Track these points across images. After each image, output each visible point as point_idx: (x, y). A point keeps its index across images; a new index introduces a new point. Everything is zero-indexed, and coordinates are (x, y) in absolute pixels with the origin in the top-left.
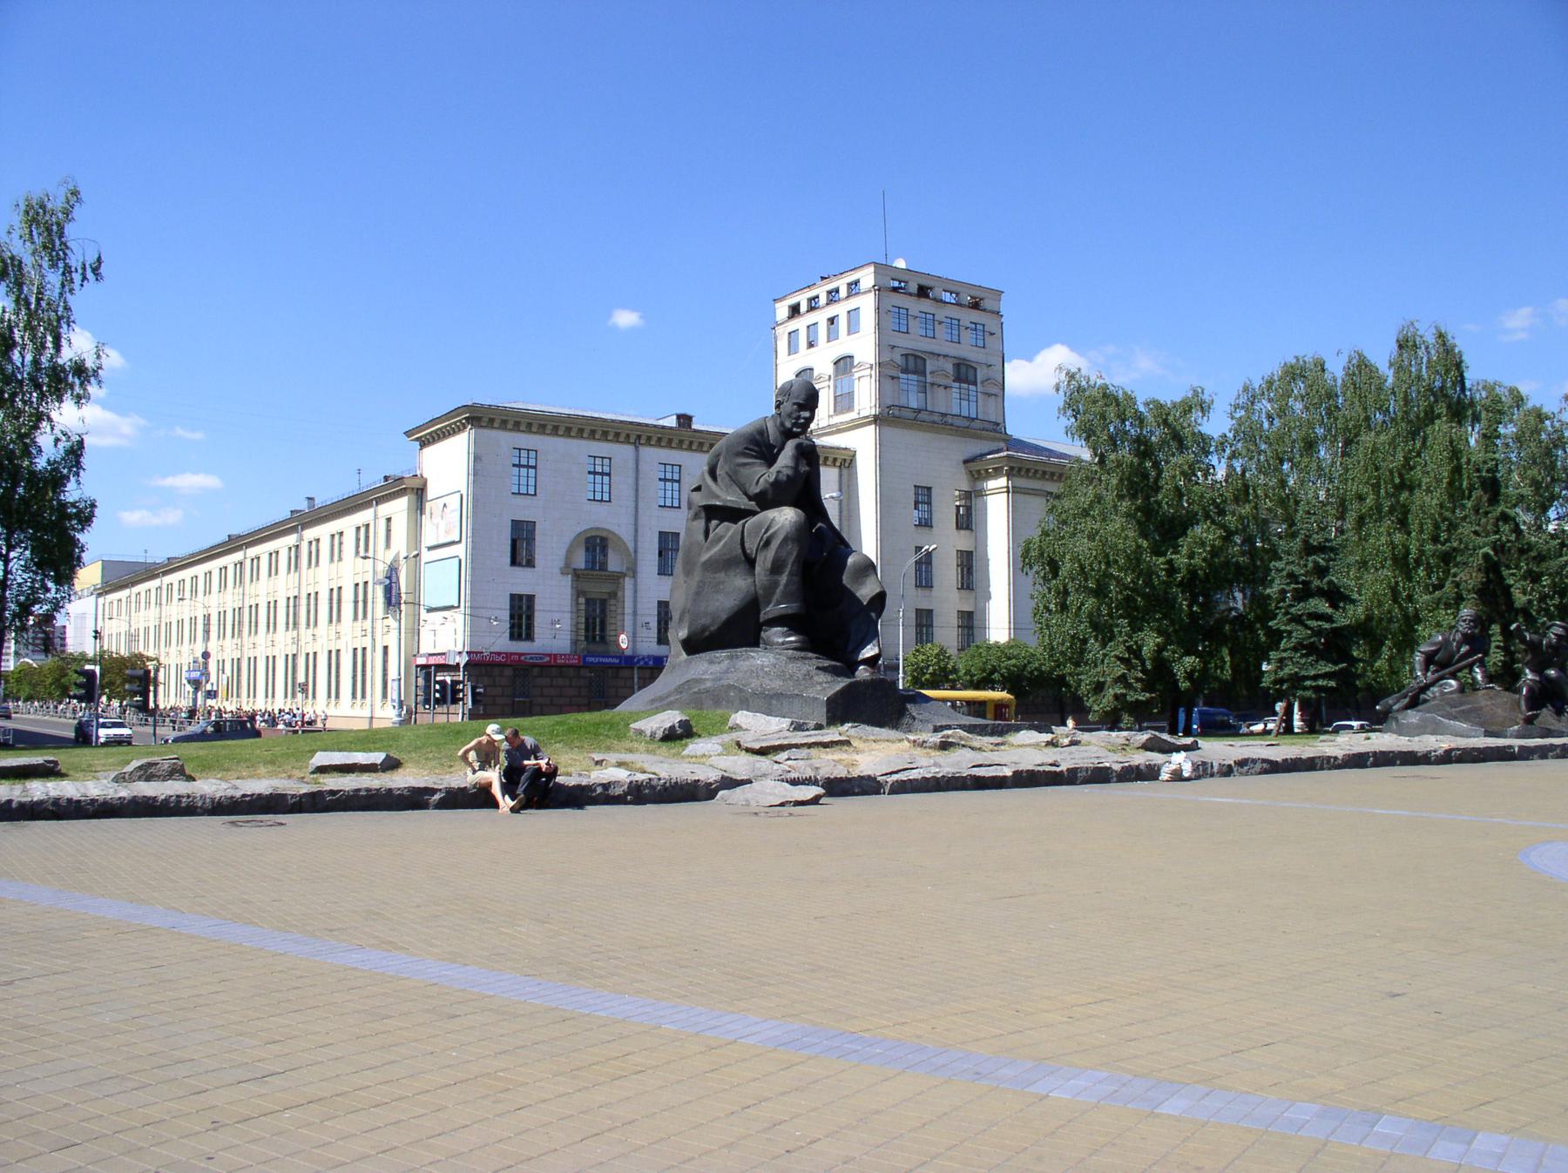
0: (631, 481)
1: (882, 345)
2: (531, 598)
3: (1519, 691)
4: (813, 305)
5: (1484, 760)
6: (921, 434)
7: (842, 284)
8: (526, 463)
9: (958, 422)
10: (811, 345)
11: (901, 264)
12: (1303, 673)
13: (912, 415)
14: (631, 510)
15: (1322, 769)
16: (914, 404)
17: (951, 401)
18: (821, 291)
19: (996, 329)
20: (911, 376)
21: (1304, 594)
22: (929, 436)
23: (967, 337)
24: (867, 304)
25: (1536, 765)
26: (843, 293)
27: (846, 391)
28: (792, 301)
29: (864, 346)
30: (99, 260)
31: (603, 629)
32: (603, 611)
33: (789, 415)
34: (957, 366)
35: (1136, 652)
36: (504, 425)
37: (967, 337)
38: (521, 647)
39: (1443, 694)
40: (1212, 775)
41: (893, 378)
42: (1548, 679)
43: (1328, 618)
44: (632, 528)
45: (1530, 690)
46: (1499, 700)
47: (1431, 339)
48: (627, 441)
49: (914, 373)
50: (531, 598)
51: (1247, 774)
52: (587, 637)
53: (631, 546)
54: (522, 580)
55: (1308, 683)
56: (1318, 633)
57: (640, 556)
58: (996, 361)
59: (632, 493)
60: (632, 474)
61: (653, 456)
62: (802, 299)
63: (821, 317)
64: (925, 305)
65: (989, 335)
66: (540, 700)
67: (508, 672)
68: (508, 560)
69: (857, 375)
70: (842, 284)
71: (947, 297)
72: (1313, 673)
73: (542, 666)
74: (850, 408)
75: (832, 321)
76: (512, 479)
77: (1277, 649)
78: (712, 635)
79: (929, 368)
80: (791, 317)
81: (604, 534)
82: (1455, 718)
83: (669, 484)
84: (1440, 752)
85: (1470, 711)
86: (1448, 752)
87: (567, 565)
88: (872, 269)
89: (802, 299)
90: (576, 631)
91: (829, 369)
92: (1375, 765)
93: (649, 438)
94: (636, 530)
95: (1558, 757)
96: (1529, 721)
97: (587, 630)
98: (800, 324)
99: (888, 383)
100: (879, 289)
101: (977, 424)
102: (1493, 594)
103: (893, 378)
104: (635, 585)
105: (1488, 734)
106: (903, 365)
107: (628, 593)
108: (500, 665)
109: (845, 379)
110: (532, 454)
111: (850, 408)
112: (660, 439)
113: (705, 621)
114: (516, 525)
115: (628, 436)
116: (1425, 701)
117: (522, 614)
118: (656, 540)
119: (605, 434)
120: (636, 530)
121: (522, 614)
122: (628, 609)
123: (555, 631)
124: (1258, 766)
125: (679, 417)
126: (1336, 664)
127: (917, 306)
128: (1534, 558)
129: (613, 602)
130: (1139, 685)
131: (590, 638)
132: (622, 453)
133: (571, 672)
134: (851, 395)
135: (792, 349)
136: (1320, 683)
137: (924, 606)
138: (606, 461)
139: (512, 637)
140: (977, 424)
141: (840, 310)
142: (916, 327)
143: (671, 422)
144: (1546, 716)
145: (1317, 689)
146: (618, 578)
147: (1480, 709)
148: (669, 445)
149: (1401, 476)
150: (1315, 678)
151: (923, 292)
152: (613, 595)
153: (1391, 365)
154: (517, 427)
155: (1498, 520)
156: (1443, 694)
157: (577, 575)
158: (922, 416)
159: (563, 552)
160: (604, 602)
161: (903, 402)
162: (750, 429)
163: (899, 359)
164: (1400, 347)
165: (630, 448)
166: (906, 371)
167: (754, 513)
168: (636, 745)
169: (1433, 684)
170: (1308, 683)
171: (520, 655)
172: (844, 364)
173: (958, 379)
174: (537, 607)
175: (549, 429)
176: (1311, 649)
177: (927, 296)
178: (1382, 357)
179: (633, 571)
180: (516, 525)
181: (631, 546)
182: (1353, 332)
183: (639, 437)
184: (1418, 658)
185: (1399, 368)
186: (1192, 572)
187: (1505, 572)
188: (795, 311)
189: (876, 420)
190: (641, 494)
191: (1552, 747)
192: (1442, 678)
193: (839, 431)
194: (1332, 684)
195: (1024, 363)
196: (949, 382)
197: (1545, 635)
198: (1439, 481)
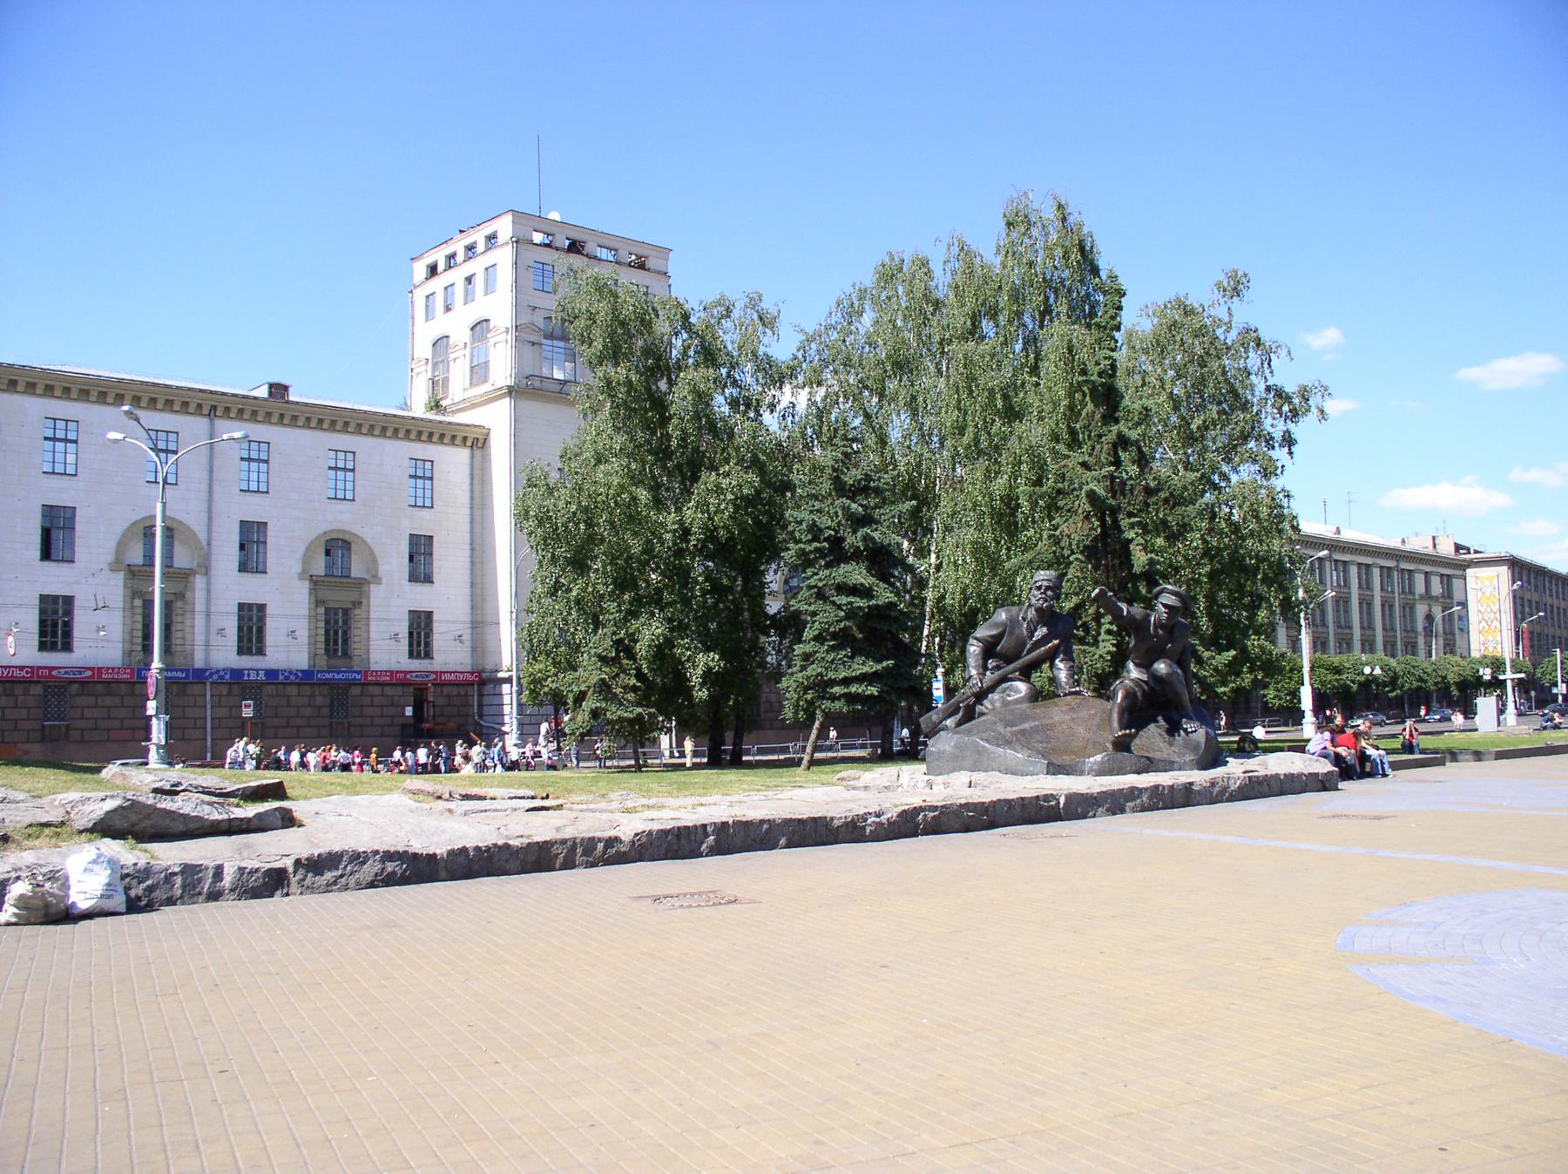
2: (429, 614)
3: (1110, 697)
5: (991, 825)
7: (479, 237)
8: (60, 436)
10: (448, 309)
11: (555, 216)
12: (831, 675)
13: (558, 387)
14: (204, 495)
15: (569, 864)
20: (556, 343)
21: (837, 553)
24: (504, 257)
25: (1100, 827)
26: (481, 247)
28: (429, 260)
29: (499, 307)
31: (345, 641)
32: (346, 622)
35: (625, 648)
36: (31, 388)
38: (246, 662)
39: (1005, 704)
40: (214, 896)
42: (1156, 678)
43: (866, 593)
44: (204, 516)
45: (1129, 695)
46: (1084, 713)
47: (1050, 213)
50: (429, 614)
51: (328, 888)
52: (327, 650)
53: (203, 537)
54: (56, 579)
55: (837, 690)
56: (852, 614)
57: (214, 550)
59: (206, 475)
61: (234, 431)
62: (439, 256)
63: (457, 276)
64: (575, 260)
66: (82, 724)
67: (37, 690)
68: (38, 554)
69: (492, 341)
70: (479, 237)
71: (604, 254)
72: (842, 675)
73: (82, 683)
76: (43, 455)
77: (800, 642)
81: (346, 537)
82: (1007, 743)
83: (254, 465)
84: (892, 814)
85: (1035, 730)
87: (304, 571)
88: (509, 218)
89: (439, 256)
90: (313, 643)
91: (466, 336)
92: (721, 849)
93: (227, 409)
94: (210, 519)
95: (1143, 809)
96: (1122, 745)
97: (327, 642)
100: (519, 242)
102: (1107, 550)
104: (208, 584)
105: (1054, 769)
108: (23, 681)
110: (72, 426)
112: (241, 411)
114: (50, 512)
115: (200, 406)
116: (981, 714)
117: (55, 623)
118: (237, 530)
119: (67, 391)
120: (210, 519)
121: (55, 623)
122: (200, 606)
123: (291, 644)
124: (370, 870)
125: (271, 386)
126: (879, 661)
128: (1166, 501)
129: (179, 604)
130: (631, 696)
131: (330, 651)
132: (192, 427)
133: (123, 689)
135: (429, 315)
136: (854, 689)
137: (250, 580)
138: (172, 437)
139: (43, 647)
141: (476, 266)
144: (1153, 737)
145: (851, 698)
147: (1052, 727)
148: (254, 417)
149: (1006, 397)
150: (846, 682)
151: (575, 247)
153: (998, 252)
154: (49, 391)
155: (1115, 446)
156: (1005, 704)
157: (315, 582)
159: (113, 544)
160: (346, 612)
161: (545, 372)
163: (541, 323)
164: (1009, 224)
165: (204, 421)
166: (551, 336)
169: (992, 689)
170: (837, 690)
171: (51, 669)
172: (480, 327)
174: (437, 628)
175: (94, 395)
176: (842, 639)
177: (579, 252)
178: (987, 242)
179: (205, 568)
180: (50, 512)
181: (203, 537)
182: (953, 222)
184: (974, 649)
185: (1010, 252)
186: (710, 533)
187: (1125, 523)
188: (433, 270)
191: (1133, 793)
192: (1004, 679)
193: (474, 406)
194: (873, 690)
197: (1152, 608)
198: (1055, 404)
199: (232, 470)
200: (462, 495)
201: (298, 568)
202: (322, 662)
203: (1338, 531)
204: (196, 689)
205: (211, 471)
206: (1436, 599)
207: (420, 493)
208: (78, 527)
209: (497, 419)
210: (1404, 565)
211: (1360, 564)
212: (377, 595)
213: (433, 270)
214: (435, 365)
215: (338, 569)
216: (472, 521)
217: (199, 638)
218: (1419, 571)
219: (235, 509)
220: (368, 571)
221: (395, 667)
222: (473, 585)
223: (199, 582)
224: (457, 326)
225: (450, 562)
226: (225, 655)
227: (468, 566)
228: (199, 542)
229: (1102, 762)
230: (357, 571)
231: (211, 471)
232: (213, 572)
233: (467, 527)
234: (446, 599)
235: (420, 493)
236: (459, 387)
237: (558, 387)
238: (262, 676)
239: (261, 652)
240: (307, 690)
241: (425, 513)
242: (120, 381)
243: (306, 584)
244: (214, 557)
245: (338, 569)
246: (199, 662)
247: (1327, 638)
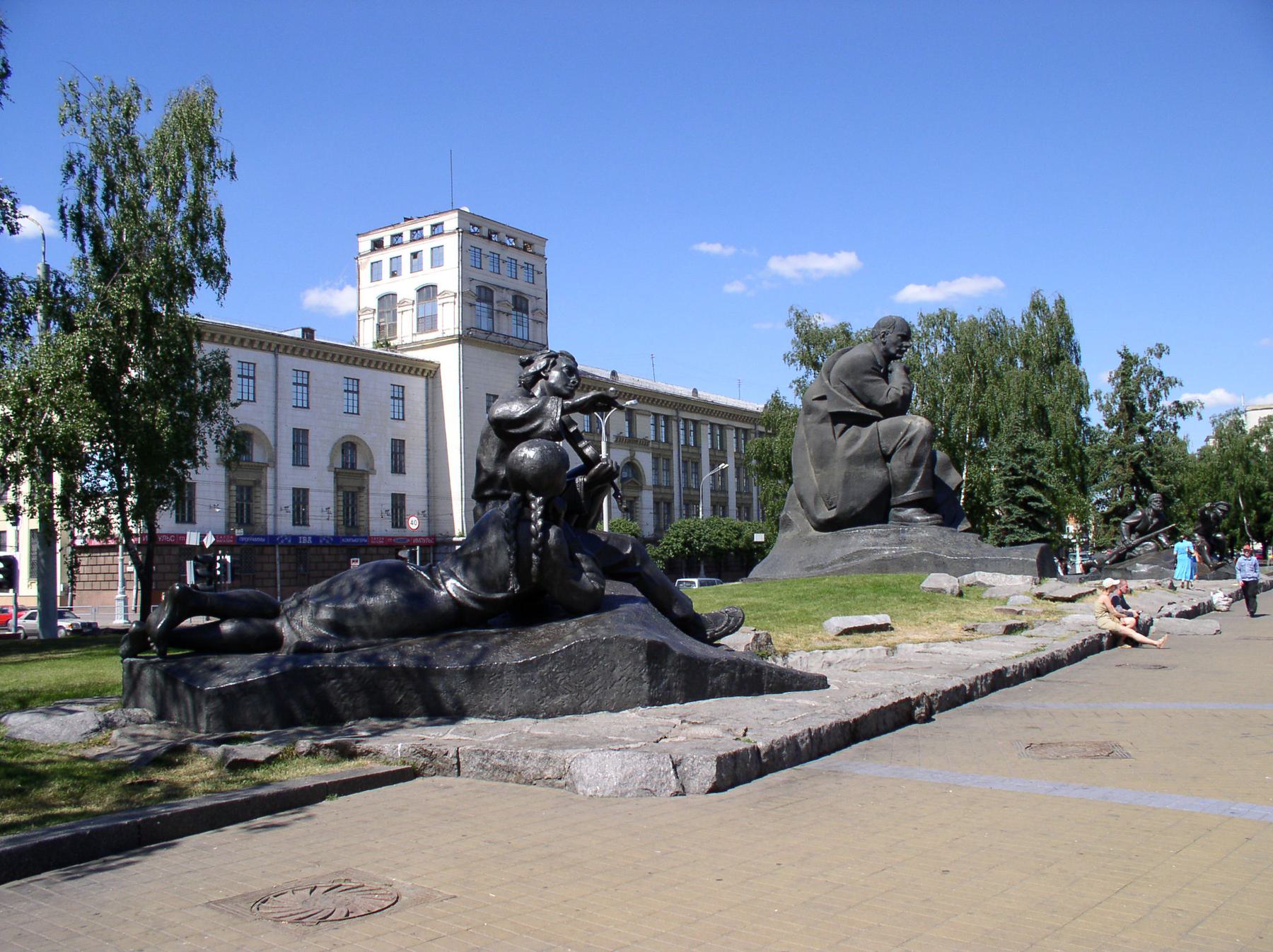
0: (271, 384)
1: (465, 278)
4: (396, 240)
6: (490, 352)
9: (516, 343)
10: (393, 274)
13: (484, 336)
14: (272, 410)
16: (484, 327)
17: (507, 325)
18: (406, 229)
19: (542, 270)
22: (495, 353)
23: (522, 274)
24: (451, 245)
27: (428, 313)
28: (376, 236)
29: (448, 278)
30: (233, 159)
33: (895, 344)
34: (515, 298)
37: (522, 274)
38: (298, 531)
41: (471, 305)
44: (272, 424)
48: (269, 349)
49: (485, 301)
53: (271, 440)
58: (542, 295)
59: (272, 395)
60: (272, 378)
61: (289, 363)
63: (405, 252)
65: (536, 273)
69: (440, 302)
71: (509, 242)
74: (433, 328)
75: (415, 255)
78: (858, 514)
79: (496, 298)
80: (373, 250)
81: (250, 430)
87: (331, 465)
91: (413, 296)
94: (276, 427)
98: (384, 256)
99: (468, 308)
100: (463, 232)
103: (471, 305)
106: (478, 295)
107: (270, 482)
109: (428, 305)
111: (433, 328)
112: (294, 349)
113: (853, 503)
120: (276, 427)
125: (305, 330)
127: (487, 247)
131: (346, 522)
137: (301, 471)
139: (294, 524)
141: (425, 247)
142: (486, 263)
143: (298, 334)
146: (261, 467)
152: (257, 483)
157: (337, 474)
158: (492, 337)
160: (249, 489)
163: (474, 290)
165: (270, 356)
166: (479, 300)
167: (878, 419)
172: (427, 292)
173: (516, 309)
179: (273, 462)
181: (271, 440)
183: (278, 346)
188: (378, 245)
189: (461, 339)
190: (280, 395)
193: (423, 347)
196: (509, 310)
199: (289, 393)
200: (422, 414)
201: (327, 463)
202: (342, 531)
203: (695, 391)
204: (268, 550)
205: (276, 392)
206: (644, 443)
207: (245, 389)
208: (311, 443)
209: (449, 360)
210: (684, 415)
211: (737, 429)
212: (374, 482)
213: (378, 245)
214: (381, 315)
215: (350, 464)
216: (427, 430)
217: (270, 509)
218: (706, 423)
219: (292, 419)
220: (367, 465)
221: (384, 534)
222: (428, 475)
223: (270, 473)
224: (405, 287)
225: (415, 458)
226: (285, 526)
227: (425, 461)
228: (268, 443)
229: (392, 610)
230: (360, 465)
231: (276, 392)
232: (279, 466)
233: (424, 434)
234: (413, 484)
235: (245, 389)
236: (406, 329)
237: (484, 336)
238: (310, 541)
239: (306, 524)
240: (334, 551)
241: (401, 424)
242: (225, 326)
243: (332, 474)
244: (279, 455)
245: (350, 464)
246: (270, 532)
247: (751, 505)
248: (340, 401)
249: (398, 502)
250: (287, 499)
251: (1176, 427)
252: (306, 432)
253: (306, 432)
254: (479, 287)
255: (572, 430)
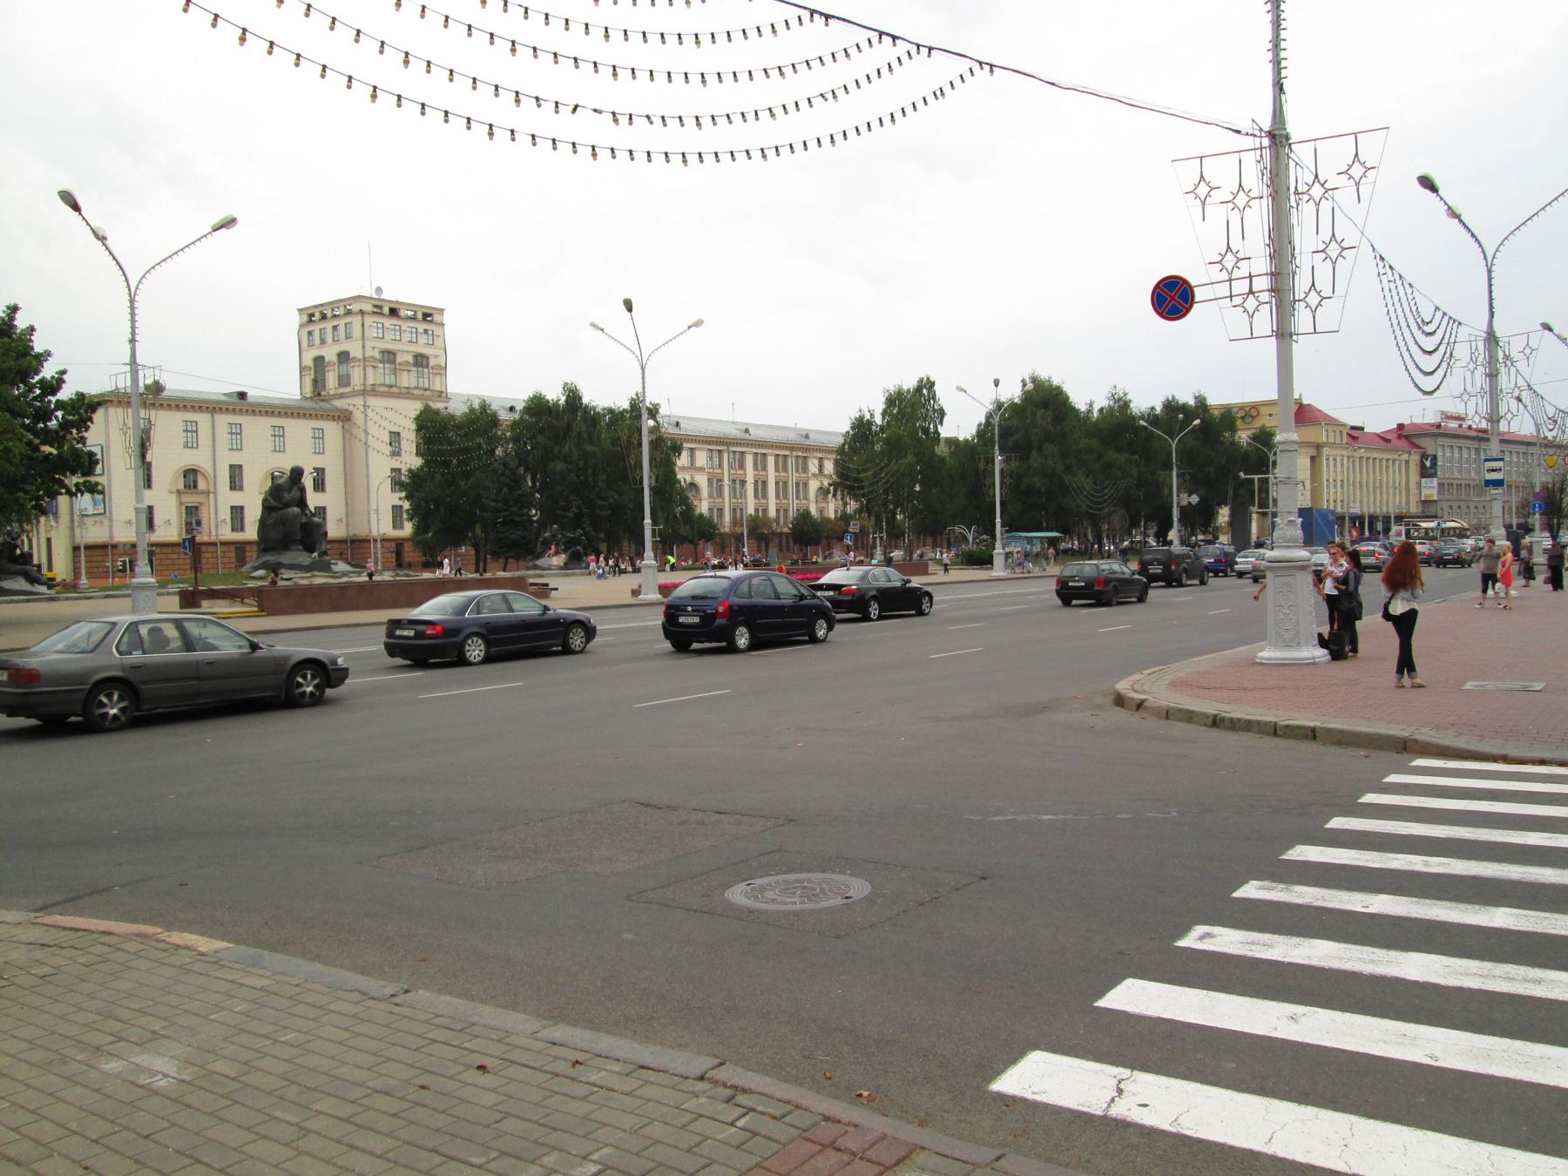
37: (423, 339)
61: (223, 420)
75: (335, 328)
86: (1090, 584)
91: (334, 358)
101: (394, 390)
111: (348, 385)
132: (203, 419)
134: (348, 376)
137: (320, 495)
140: (394, 390)
162: (202, 397)
165: (208, 416)
168: (573, 590)
195: (1087, 394)
206: (702, 469)
224: (330, 354)
226: (227, 534)
239: (242, 529)
248: (309, 444)
249: (238, 512)
250: (225, 514)
251: (1470, 427)
252: (240, 467)
253: (240, 467)
254: (383, 352)
255: (1195, 499)
